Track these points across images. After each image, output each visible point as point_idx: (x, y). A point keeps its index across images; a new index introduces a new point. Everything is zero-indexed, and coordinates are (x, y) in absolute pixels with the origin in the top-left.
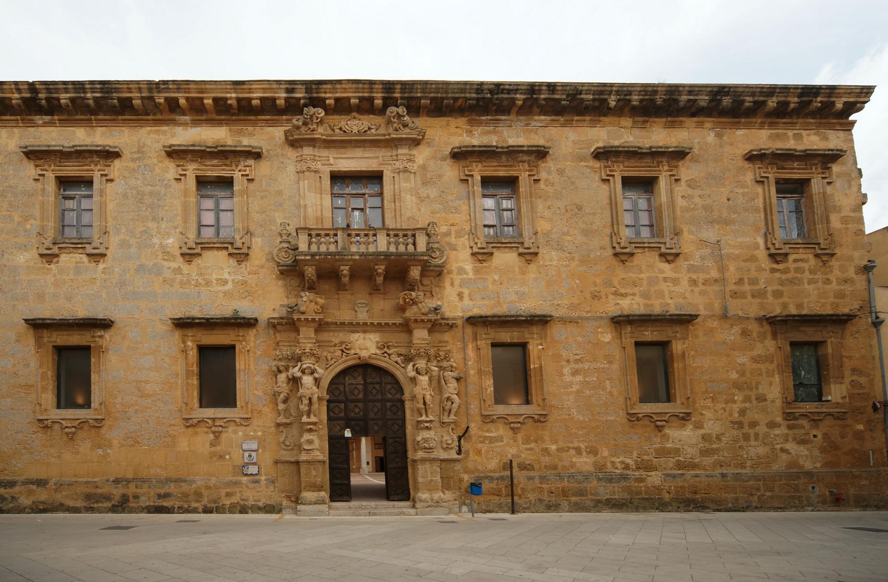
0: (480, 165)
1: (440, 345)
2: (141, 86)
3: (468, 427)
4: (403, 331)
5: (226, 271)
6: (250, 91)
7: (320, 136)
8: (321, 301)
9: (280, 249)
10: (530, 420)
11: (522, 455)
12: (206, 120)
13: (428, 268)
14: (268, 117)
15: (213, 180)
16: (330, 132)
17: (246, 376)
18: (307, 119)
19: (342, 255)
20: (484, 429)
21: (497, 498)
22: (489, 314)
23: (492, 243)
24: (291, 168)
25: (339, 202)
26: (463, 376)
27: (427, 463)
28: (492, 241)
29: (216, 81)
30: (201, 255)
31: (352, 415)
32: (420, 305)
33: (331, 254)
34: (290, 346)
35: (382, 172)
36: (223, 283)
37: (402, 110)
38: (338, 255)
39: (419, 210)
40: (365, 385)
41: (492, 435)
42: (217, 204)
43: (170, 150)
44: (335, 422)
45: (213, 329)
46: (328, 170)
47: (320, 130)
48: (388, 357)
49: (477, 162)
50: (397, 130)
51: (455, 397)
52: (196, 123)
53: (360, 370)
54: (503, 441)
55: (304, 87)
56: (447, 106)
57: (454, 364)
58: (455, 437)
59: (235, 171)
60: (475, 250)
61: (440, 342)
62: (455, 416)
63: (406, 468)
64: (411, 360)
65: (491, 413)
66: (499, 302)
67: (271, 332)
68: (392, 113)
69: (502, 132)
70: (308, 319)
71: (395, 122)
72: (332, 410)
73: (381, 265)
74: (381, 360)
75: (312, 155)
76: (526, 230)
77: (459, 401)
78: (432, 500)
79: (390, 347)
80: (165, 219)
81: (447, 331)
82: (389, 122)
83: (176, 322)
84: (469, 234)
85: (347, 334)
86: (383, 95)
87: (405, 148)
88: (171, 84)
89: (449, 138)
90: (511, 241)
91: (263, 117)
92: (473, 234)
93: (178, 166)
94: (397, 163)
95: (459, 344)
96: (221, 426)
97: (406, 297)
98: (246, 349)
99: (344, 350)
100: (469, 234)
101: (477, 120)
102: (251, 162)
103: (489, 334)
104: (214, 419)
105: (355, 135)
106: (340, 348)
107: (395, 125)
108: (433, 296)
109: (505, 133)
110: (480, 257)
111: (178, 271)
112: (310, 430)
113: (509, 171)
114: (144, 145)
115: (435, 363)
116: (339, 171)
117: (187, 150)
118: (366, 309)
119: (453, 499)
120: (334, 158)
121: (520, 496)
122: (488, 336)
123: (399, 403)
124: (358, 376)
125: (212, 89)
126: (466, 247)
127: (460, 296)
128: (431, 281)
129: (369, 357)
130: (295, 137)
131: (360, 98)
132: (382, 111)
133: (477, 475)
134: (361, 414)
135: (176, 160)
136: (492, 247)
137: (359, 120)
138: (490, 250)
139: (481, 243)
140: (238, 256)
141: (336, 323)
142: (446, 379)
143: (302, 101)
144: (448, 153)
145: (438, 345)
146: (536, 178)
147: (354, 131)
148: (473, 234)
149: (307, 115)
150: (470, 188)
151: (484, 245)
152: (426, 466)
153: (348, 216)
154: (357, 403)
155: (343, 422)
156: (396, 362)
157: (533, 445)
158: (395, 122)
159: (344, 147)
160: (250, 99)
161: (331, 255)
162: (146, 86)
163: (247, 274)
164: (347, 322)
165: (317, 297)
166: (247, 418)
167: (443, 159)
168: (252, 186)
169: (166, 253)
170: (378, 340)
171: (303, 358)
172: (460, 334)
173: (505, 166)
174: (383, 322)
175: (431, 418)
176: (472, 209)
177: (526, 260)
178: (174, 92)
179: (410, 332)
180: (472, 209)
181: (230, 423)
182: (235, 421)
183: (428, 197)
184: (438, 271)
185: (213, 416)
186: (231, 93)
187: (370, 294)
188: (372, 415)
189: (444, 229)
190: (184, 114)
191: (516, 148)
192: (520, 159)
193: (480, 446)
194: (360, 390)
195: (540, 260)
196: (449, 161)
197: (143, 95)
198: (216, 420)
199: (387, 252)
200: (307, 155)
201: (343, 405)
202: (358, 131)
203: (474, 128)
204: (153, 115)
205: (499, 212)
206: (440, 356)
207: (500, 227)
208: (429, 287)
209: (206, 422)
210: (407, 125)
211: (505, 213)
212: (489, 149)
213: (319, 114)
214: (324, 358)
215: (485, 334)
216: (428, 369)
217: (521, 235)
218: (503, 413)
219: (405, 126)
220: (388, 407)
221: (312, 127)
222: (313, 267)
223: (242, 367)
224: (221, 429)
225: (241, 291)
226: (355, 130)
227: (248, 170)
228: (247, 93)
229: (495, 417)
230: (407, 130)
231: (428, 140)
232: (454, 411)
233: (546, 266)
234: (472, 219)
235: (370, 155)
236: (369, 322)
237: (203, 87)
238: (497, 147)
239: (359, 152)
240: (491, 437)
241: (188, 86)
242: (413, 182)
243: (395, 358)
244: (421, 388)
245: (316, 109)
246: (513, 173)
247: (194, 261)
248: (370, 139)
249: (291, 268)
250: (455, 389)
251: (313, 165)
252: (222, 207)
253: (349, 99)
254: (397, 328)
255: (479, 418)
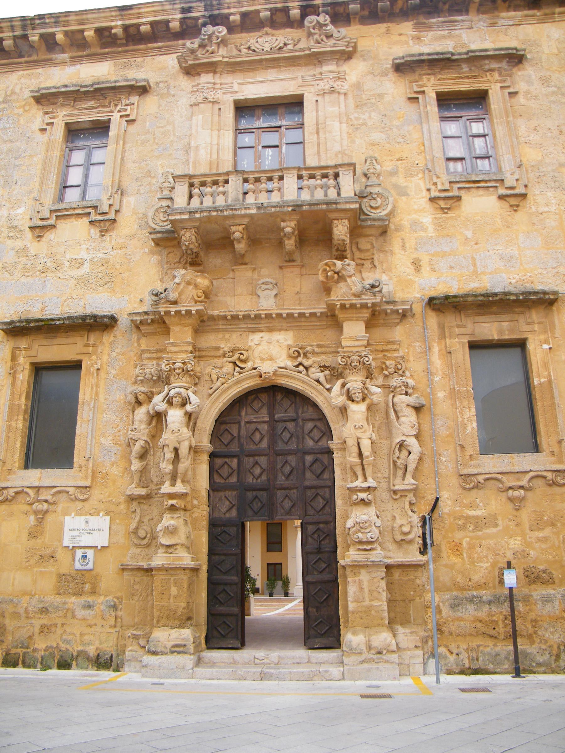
0: (433, 78)
1: (389, 347)
2: (13, 23)
3: (437, 499)
4: (329, 327)
5: (84, 246)
6: (139, 15)
7: (220, 59)
8: (203, 281)
9: (157, 210)
10: (540, 482)
11: (532, 553)
12: (87, 56)
13: (364, 224)
14: (160, 44)
15: (87, 126)
16: (235, 52)
17: (91, 413)
18: (204, 40)
19: (232, 209)
20: (465, 502)
21: (490, 643)
22: (461, 292)
23: (458, 182)
24: (184, 101)
25: (247, 140)
26: (424, 403)
27: (363, 571)
28: (458, 180)
29: (100, 9)
30: (55, 227)
31: (250, 479)
32: (348, 280)
33: (216, 209)
34: (157, 359)
35: (302, 96)
36: (77, 265)
37: (323, 18)
38: (226, 210)
39: (353, 142)
40: (273, 423)
41: (478, 513)
42: (89, 156)
43: (39, 94)
44: (222, 494)
45: (55, 337)
46: (232, 99)
47: (223, 51)
48: (304, 372)
49: (429, 74)
50: (319, 43)
51: (412, 442)
52: (75, 60)
53: (264, 397)
54: (496, 525)
55: (203, 4)
56: (383, 11)
57: (411, 382)
58: (416, 519)
59: (113, 112)
60: (434, 194)
61: (388, 343)
62: (414, 477)
63: (335, 581)
64: (340, 375)
65: (475, 471)
66: (475, 272)
67: (135, 336)
68: (311, 22)
69: (460, 36)
70: (180, 312)
71: (315, 34)
72: (217, 471)
73: (291, 221)
74: (293, 378)
75: (211, 83)
76: (506, 162)
77: (420, 449)
78: (370, 648)
79: (309, 355)
80: (19, 183)
81: (398, 324)
82: (310, 35)
83: (5, 327)
84: (424, 171)
85: (244, 335)
86: (300, 3)
87: (332, 64)
88: (48, 18)
89: (390, 48)
90: (487, 179)
91: (155, 45)
92: (430, 171)
93: (46, 113)
94: (321, 83)
95: (418, 346)
96: (46, 501)
97: (328, 269)
98: (96, 367)
99: (238, 363)
100: (424, 171)
101: (425, 23)
102: (134, 99)
103: (465, 326)
104: (38, 489)
105: (268, 53)
106: (230, 359)
107: (316, 37)
108: (375, 266)
109: (464, 36)
110: (442, 204)
111: (23, 252)
112: (173, 508)
113: (474, 83)
114: (13, 92)
115: (380, 381)
116: (246, 99)
117: (58, 92)
118: (274, 292)
119: (412, 645)
120: (240, 84)
121: (530, 637)
122: (462, 330)
123: (326, 455)
124: (261, 407)
125: (94, 19)
126: (421, 191)
127: (417, 265)
128: (372, 244)
129: (275, 373)
130: (190, 62)
131: (271, 10)
132: (300, 23)
133: (455, 593)
134: (264, 477)
135: (45, 107)
136: (459, 188)
137: (273, 35)
138: (455, 193)
139: (443, 184)
140: (102, 224)
141: (225, 317)
142: (397, 409)
143: (200, 21)
144: (389, 66)
145: (385, 348)
146: (511, 90)
147: (265, 49)
148: (430, 171)
149: (204, 35)
150: (422, 108)
151: (447, 186)
152: (361, 577)
153: (258, 157)
154: (257, 458)
155: (234, 493)
156: (318, 381)
157: (547, 532)
158: (315, 34)
159: (254, 70)
160: (138, 25)
161: (217, 211)
162: (19, 23)
163: (110, 250)
164: (241, 314)
165: (197, 276)
166: (86, 487)
167: (384, 74)
168: (132, 129)
169: (13, 228)
170: (290, 342)
171: (172, 379)
172: (418, 329)
173: (468, 77)
174: (296, 312)
175: (371, 483)
176: (426, 136)
177: (511, 206)
178: (51, 27)
179: (338, 326)
180: (426, 136)
181: (61, 495)
182: (68, 492)
183: (365, 124)
184: (380, 227)
185: (36, 484)
186: (117, 21)
187: (281, 268)
188: (281, 480)
189: (388, 166)
190: (63, 51)
191: (477, 54)
192: (487, 67)
193: (459, 535)
194: (264, 432)
195: (531, 205)
196: (392, 76)
197: (16, 33)
198: (41, 490)
199: (297, 201)
200: (205, 83)
201: (235, 460)
202: (271, 49)
203: (422, 33)
204: (28, 57)
205: (468, 140)
206: (387, 368)
207: (471, 159)
208: (369, 254)
209: (27, 493)
210: (332, 36)
211: (476, 140)
212: (441, 56)
213: (220, 32)
214: (207, 378)
215: (458, 326)
216: (366, 392)
217: (500, 169)
218: (494, 470)
219: (329, 36)
220: (307, 464)
221: (210, 49)
222: (193, 230)
223: (87, 397)
224: (45, 506)
225: (100, 275)
226: (267, 48)
227: (129, 110)
228: (134, 18)
229: (481, 478)
230: (332, 41)
231: (362, 53)
232: (411, 467)
233: (541, 214)
234: (427, 149)
235: (287, 76)
236: (274, 312)
237: (84, 17)
238: (452, 54)
239: (272, 74)
240: (477, 517)
241: (66, 19)
242: (342, 106)
243: (316, 373)
244: (352, 426)
245: (216, 28)
246: (479, 86)
247: (46, 235)
248: (285, 57)
249: (165, 235)
250: (412, 427)
251: (211, 96)
252: (95, 160)
253: (258, 12)
254: (320, 321)
255: (455, 481)
